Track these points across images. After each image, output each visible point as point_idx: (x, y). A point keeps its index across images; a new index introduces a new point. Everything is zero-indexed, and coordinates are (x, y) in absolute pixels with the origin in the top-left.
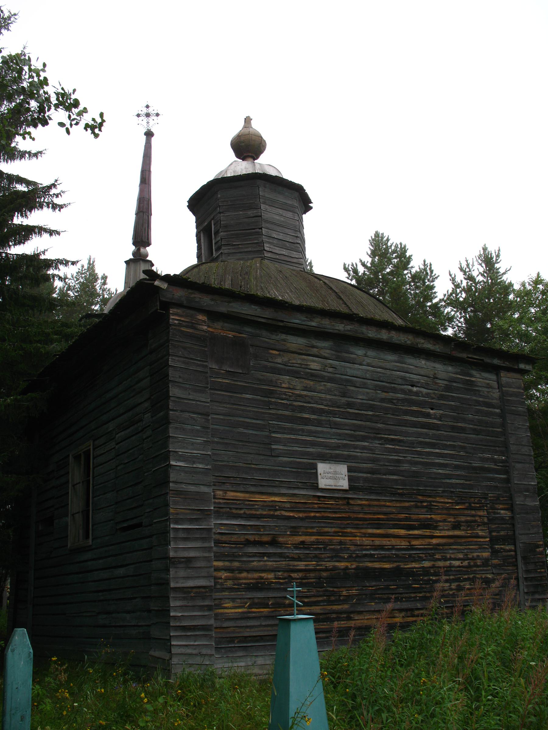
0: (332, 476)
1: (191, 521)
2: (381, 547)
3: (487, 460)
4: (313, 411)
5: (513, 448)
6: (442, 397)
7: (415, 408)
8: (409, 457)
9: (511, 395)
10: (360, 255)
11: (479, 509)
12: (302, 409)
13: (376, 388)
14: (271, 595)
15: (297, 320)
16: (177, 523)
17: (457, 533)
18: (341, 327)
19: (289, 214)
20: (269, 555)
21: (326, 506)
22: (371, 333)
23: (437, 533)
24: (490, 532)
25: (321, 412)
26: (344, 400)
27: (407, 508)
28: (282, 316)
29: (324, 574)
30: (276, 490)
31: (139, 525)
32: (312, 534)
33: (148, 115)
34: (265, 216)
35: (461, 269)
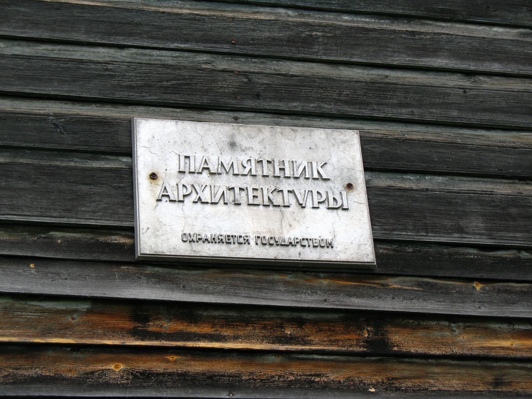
21: (197, 367)
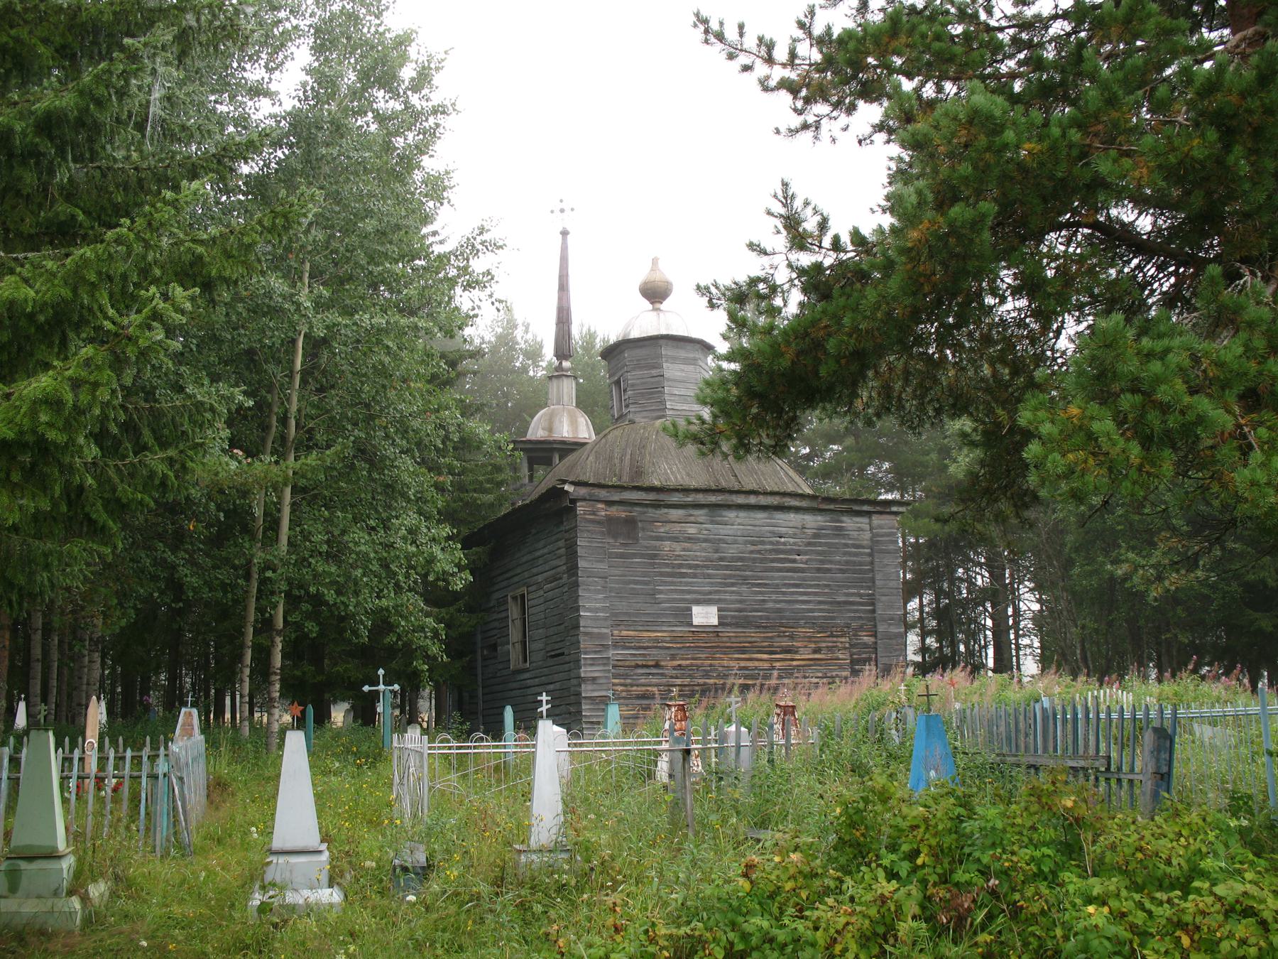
0: (705, 616)
1: (596, 652)
3: (853, 594)
4: (690, 567)
6: (809, 544)
11: (842, 636)
12: (680, 566)
13: (746, 543)
15: (676, 498)
16: (586, 653)
17: (817, 656)
18: (713, 499)
20: (653, 674)
23: (798, 657)
25: (697, 566)
26: (716, 555)
31: (563, 654)
33: (562, 211)
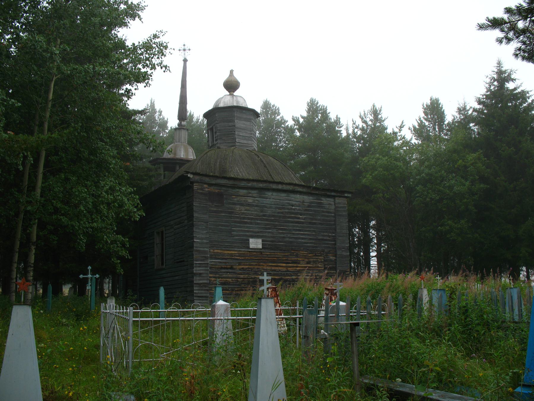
0: (255, 243)
1: (201, 260)
2: (275, 270)
4: (249, 219)
5: (338, 230)
6: (306, 210)
7: (293, 215)
8: (289, 235)
9: (340, 208)
10: (301, 112)
11: (320, 256)
12: (244, 218)
13: (276, 208)
14: (230, 286)
18: (261, 185)
19: (248, 123)
20: (230, 272)
22: (274, 186)
23: (299, 265)
24: (324, 266)
25: (252, 219)
26: (261, 214)
27: (287, 255)
28: (236, 183)
29: (251, 280)
30: (233, 249)
31: (184, 261)
32: (246, 265)
33: (184, 50)
34: (237, 125)
35: (360, 117)
